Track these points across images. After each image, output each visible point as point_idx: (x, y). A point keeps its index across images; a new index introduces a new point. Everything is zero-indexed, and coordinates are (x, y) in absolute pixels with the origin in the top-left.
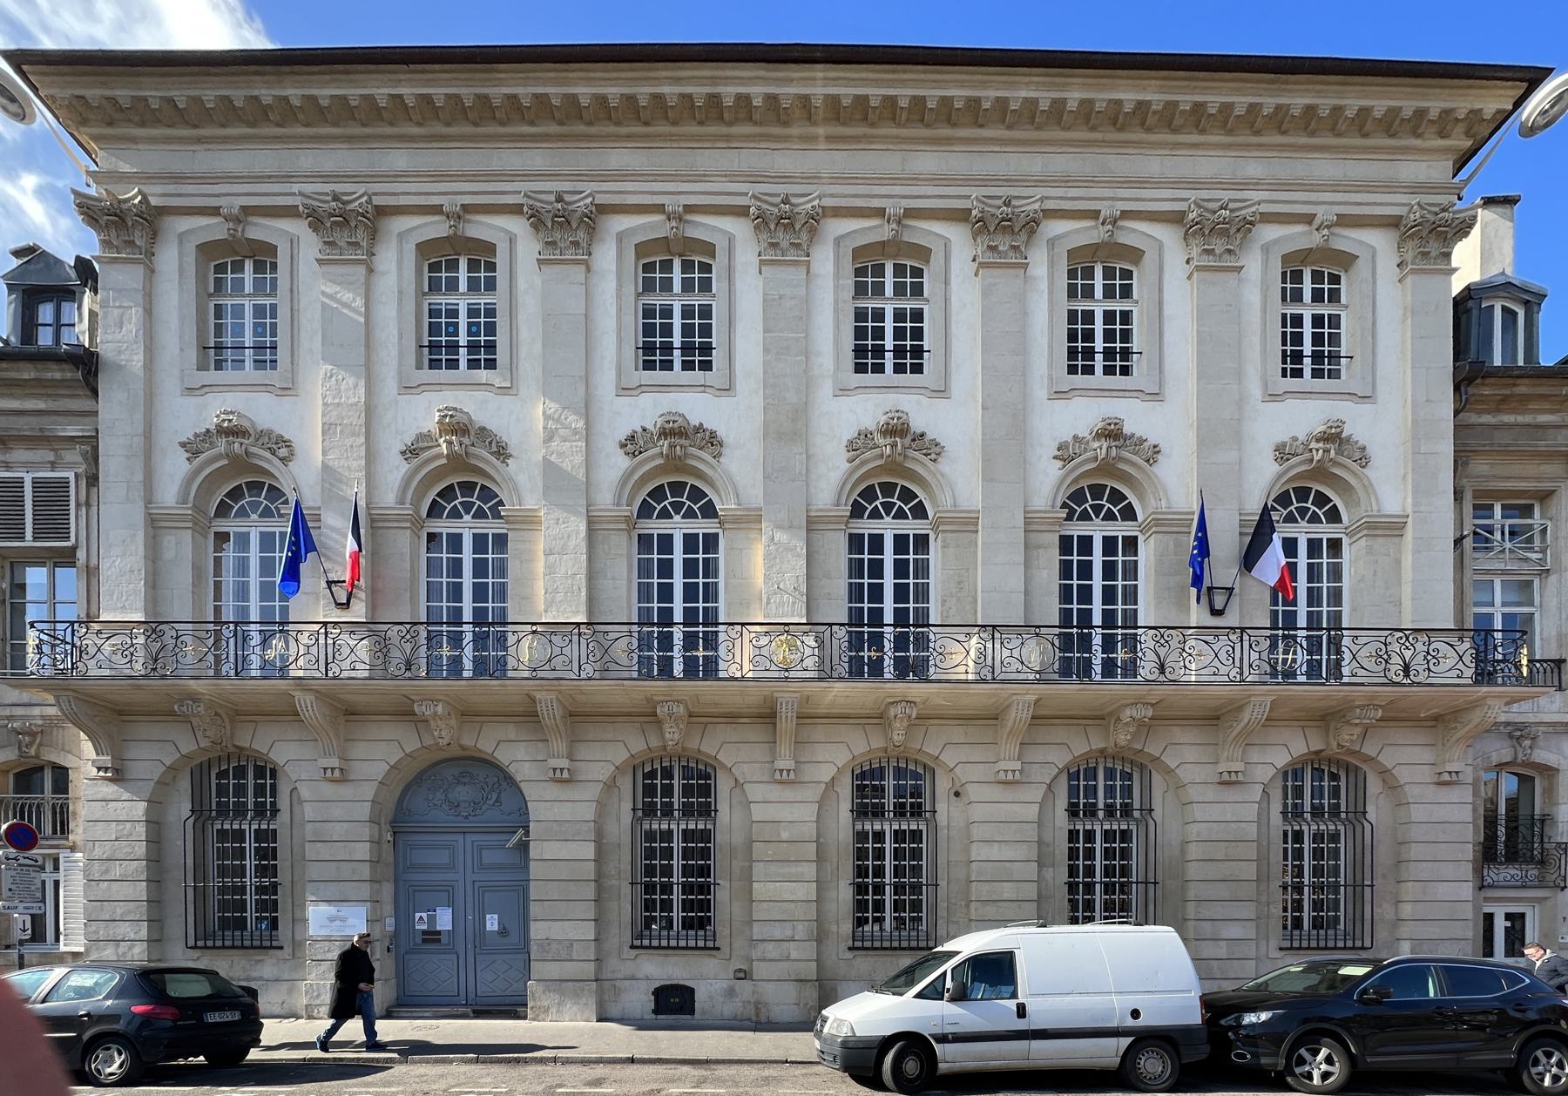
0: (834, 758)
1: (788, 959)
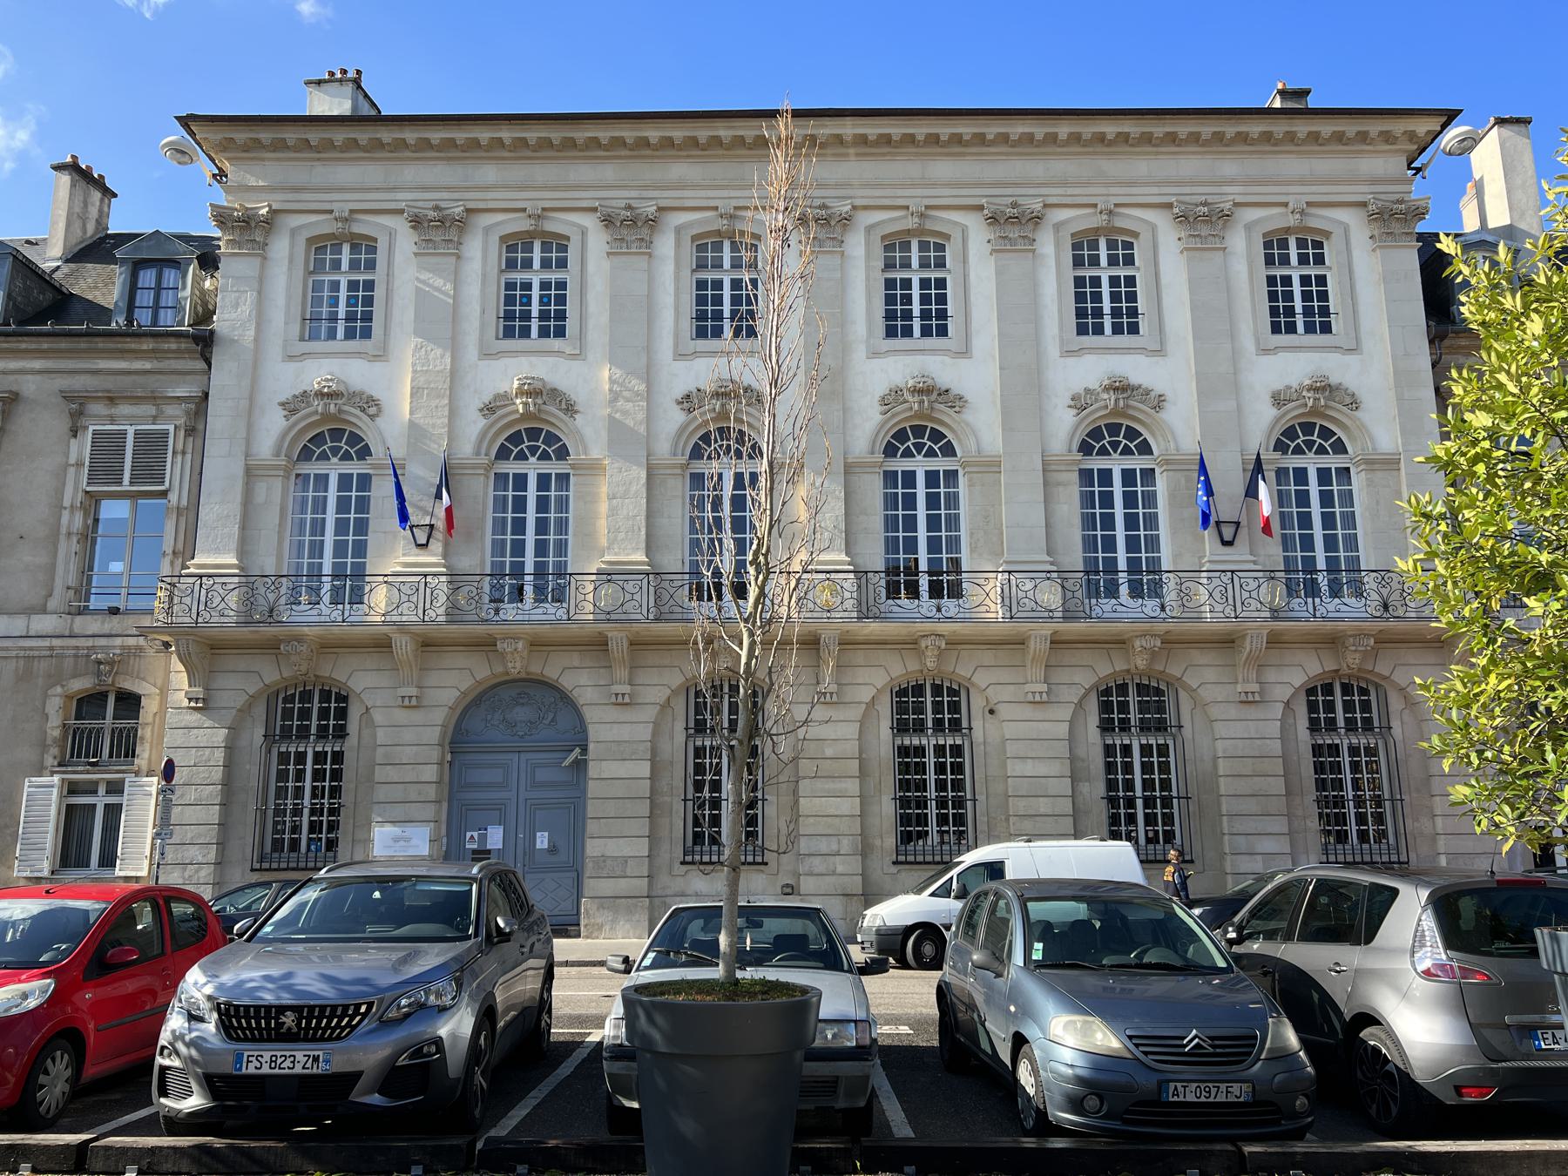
0: (874, 681)
1: (834, 873)
